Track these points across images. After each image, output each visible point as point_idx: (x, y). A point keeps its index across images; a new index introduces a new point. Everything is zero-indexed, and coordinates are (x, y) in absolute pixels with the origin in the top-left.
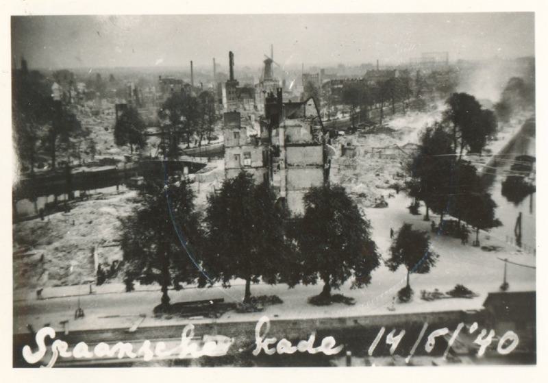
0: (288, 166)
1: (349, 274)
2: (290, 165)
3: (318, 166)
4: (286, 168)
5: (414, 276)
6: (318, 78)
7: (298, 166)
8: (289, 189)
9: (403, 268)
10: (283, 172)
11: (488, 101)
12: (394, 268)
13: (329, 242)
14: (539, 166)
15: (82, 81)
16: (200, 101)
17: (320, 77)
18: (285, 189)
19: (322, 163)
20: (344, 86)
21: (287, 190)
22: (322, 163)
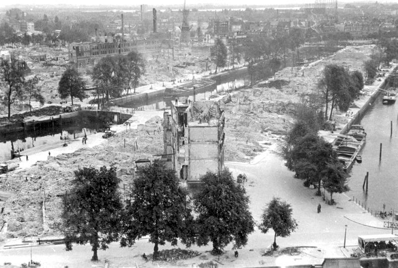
0: (190, 142)
1: (231, 239)
2: (192, 141)
3: (214, 142)
4: (189, 143)
5: (279, 238)
6: (227, 24)
7: (199, 141)
8: (191, 158)
9: (271, 232)
10: (186, 146)
11: (199, 78)
12: (265, 231)
13: (222, 213)
14: (307, 3)
15: (30, 20)
16: (32, 38)
17: (229, 24)
18: (188, 159)
19: (217, 140)
20: (247, 37)
21: (189, 160)
22: (217, 140)
